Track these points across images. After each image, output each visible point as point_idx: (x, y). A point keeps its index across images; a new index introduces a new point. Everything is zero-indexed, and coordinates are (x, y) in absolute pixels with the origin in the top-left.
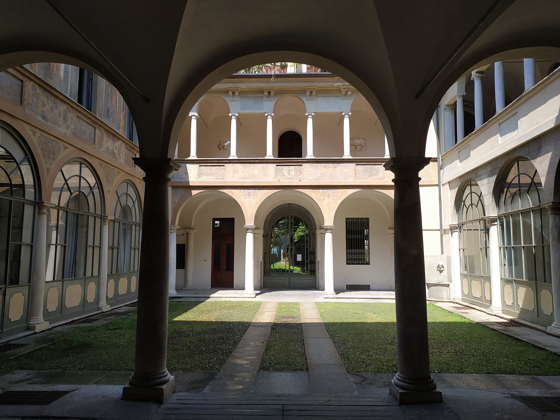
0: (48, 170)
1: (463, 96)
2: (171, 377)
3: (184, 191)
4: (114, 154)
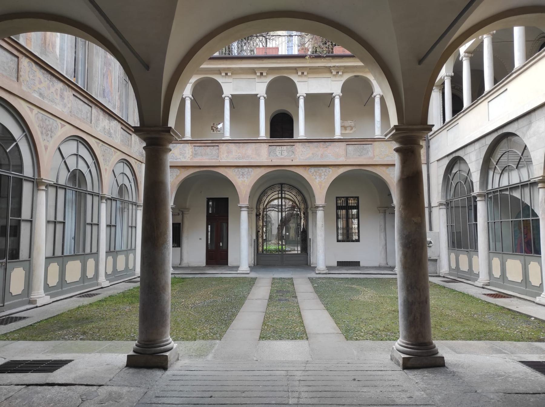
0: (46, 148)
1: (452, 77)
2: (174, 345)
3: (179, 171)
4: (110, 134)
